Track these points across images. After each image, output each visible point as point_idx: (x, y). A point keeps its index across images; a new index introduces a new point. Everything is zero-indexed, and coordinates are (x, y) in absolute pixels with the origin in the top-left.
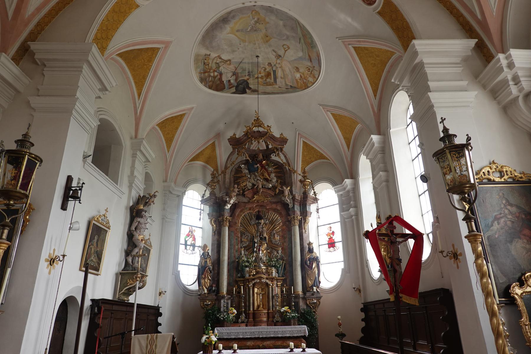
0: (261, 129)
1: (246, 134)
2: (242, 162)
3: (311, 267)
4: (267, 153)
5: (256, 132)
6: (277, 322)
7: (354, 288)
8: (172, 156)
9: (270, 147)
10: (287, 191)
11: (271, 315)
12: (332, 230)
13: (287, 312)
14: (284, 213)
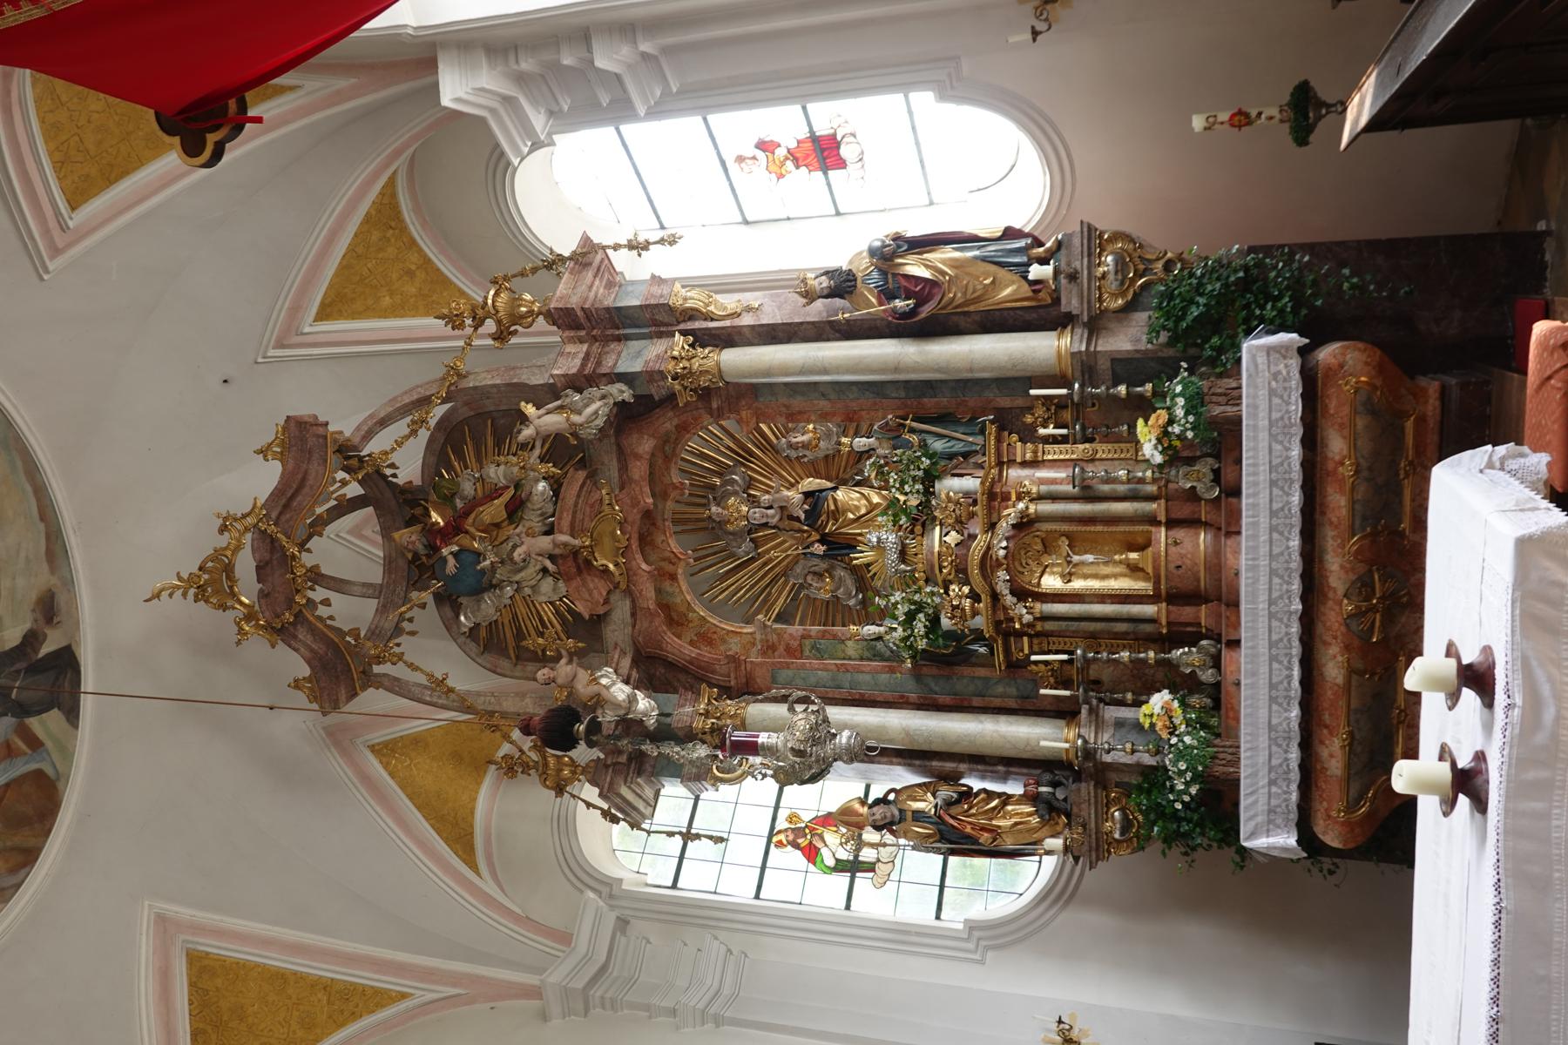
0: (245, 565)
1: (281, 632)
2: (451, 625)
3: (922, 290)
4: (394, 503)
5: (262, 583)
6: (1217, 476)
7: (1035, 34)
8: (429, 975)
9: (354, 490)
10: (542, 420)
11: (1184, 511)
12: (750, 150)
13: (1165, 433)
14: (667, 422)
